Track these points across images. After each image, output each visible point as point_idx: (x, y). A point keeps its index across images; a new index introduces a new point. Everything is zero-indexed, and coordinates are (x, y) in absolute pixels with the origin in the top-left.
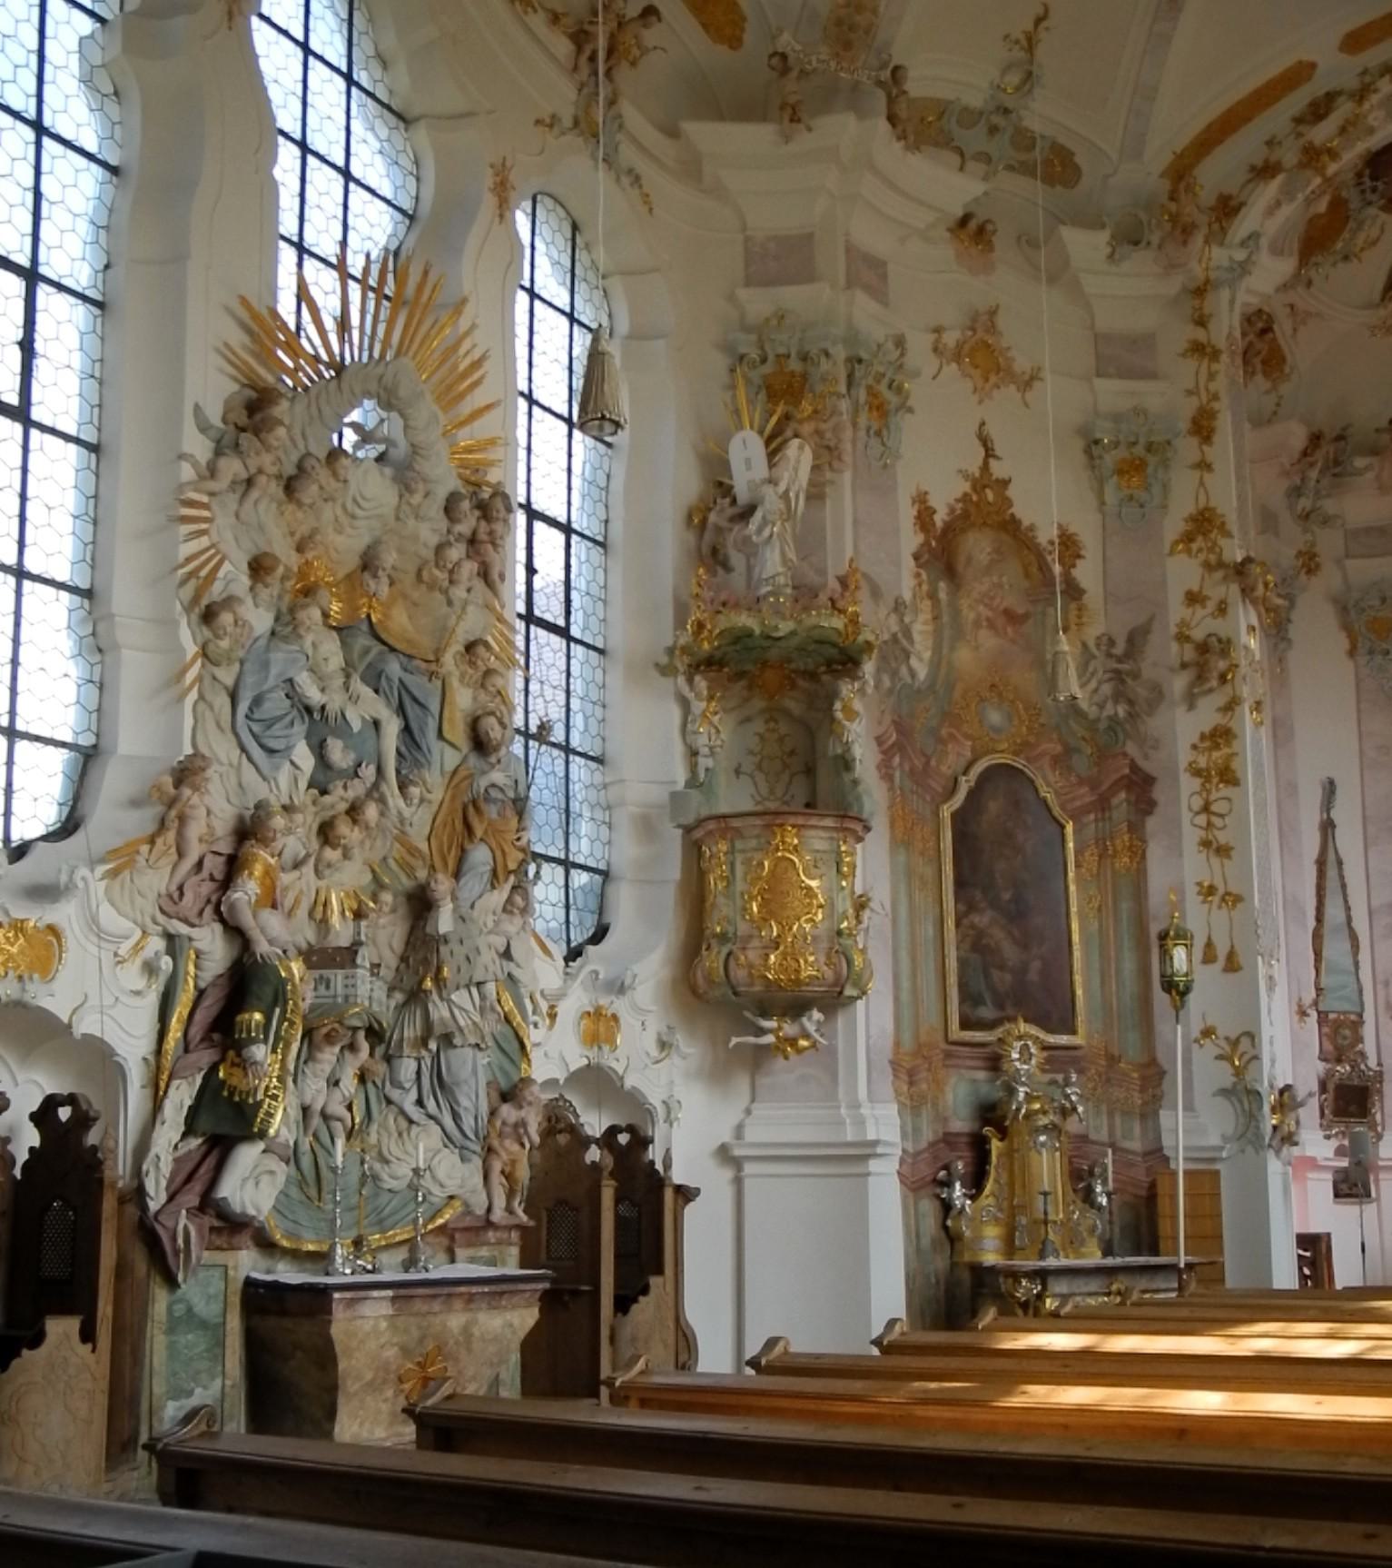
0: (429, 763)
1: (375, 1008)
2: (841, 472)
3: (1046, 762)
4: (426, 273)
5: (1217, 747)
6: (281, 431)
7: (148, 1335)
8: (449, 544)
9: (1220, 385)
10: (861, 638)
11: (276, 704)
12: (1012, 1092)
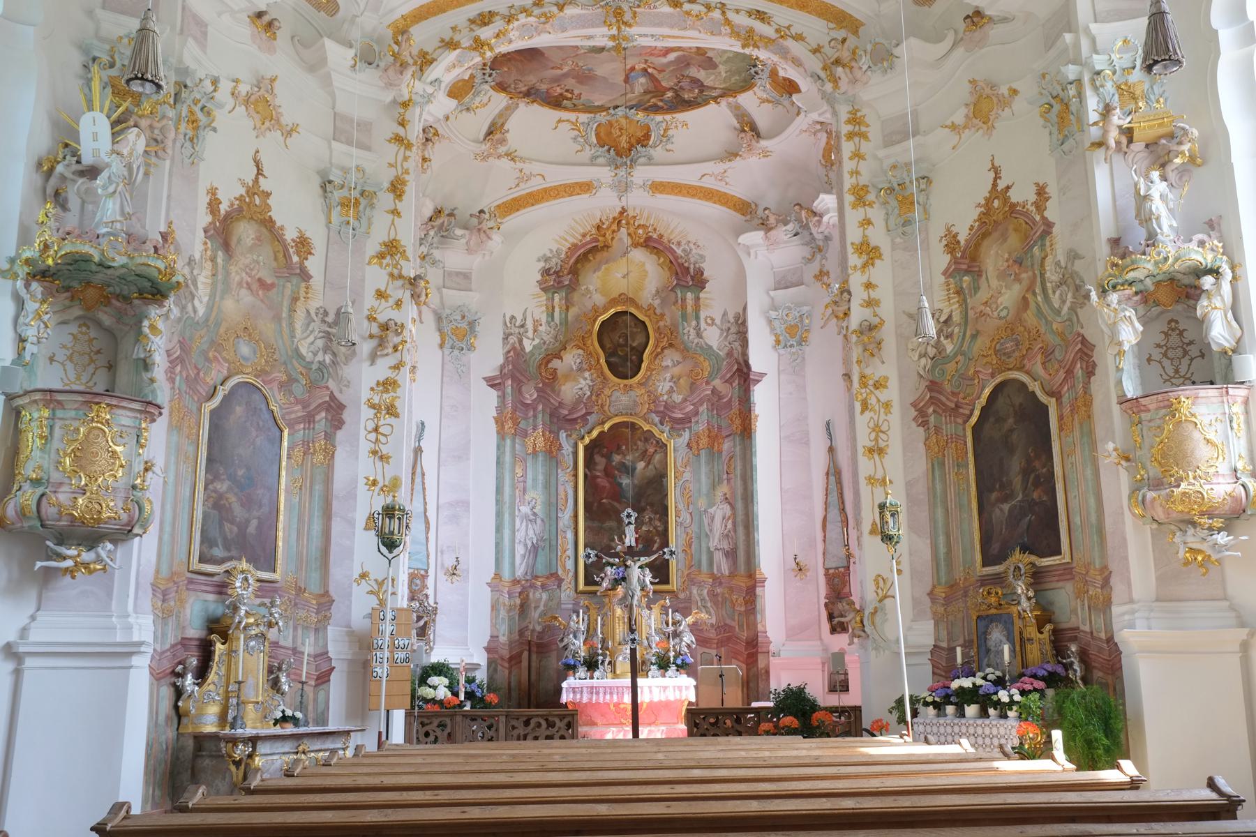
5: (387, 391)
9: (410, 165)
10: (174, 279)
12: (235, 609)
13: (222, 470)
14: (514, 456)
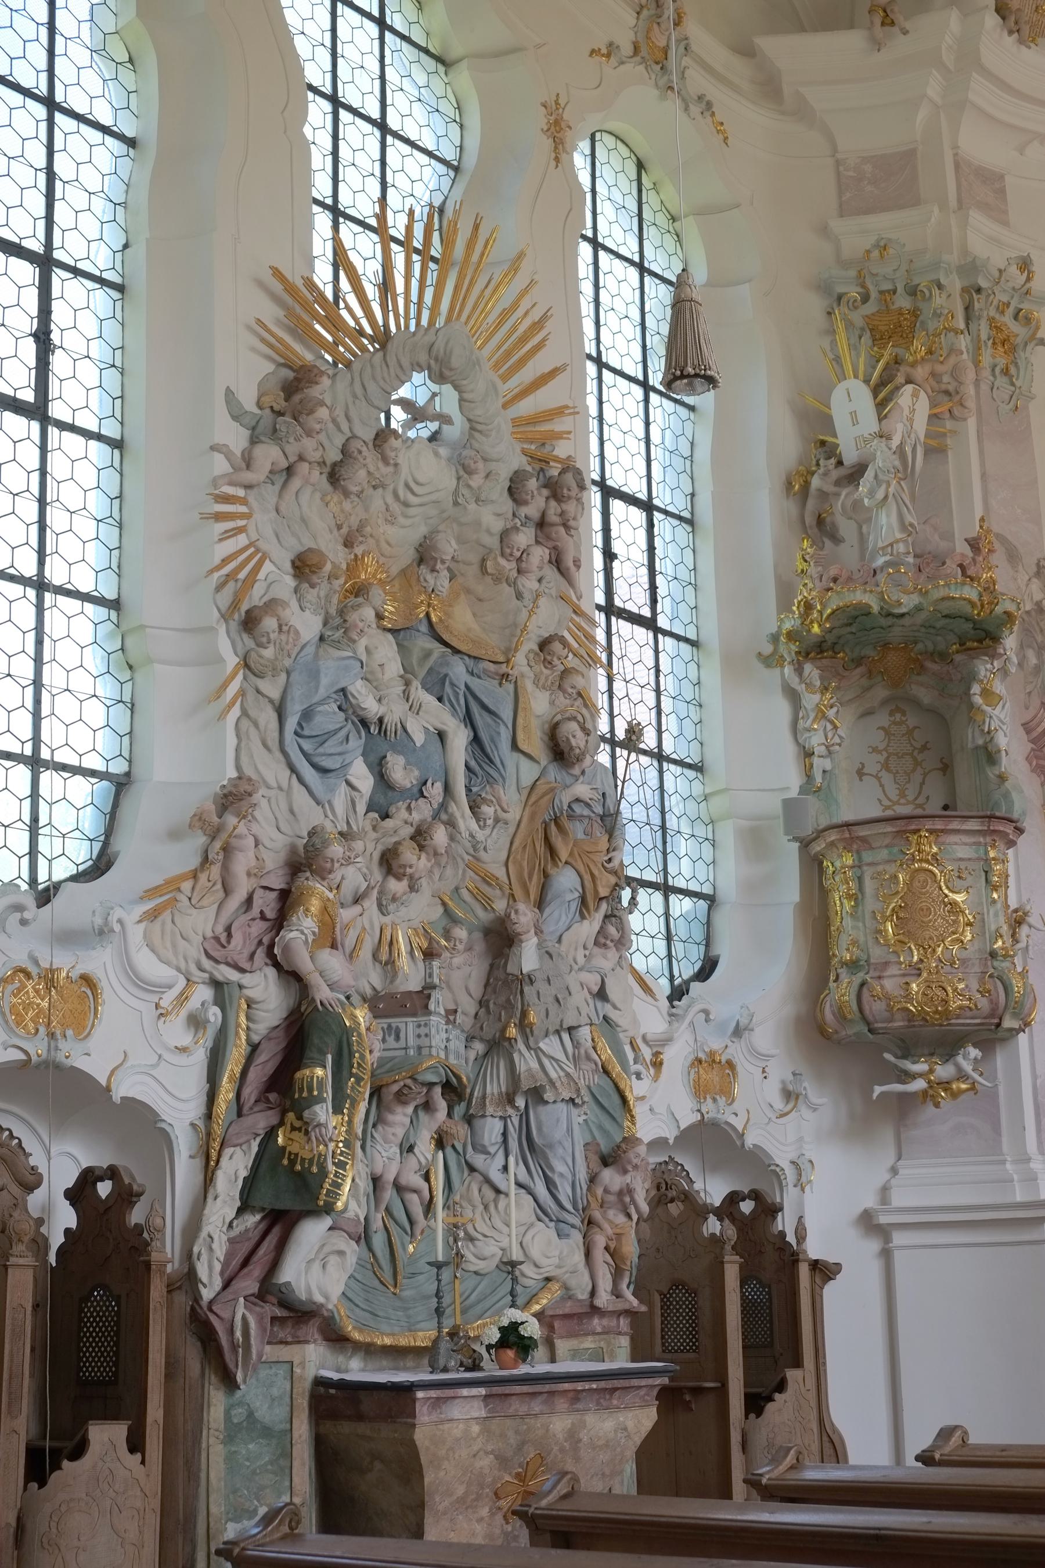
0: (504, 779)
1: (452, 1061)
2: (965, 419)
4: (476, 227)
6: (323, 413)
7: (204, 1445)
8: (516, 529)
10: (999, 609)
11: (330, 717)
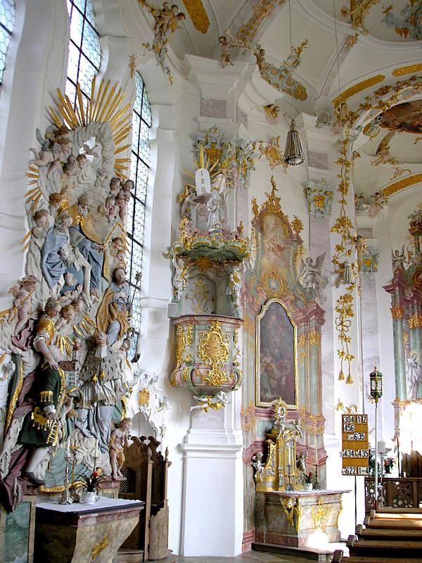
3: (289, 302)
5: (346, 302)
13: (267, 351)
14: (403, 331)
